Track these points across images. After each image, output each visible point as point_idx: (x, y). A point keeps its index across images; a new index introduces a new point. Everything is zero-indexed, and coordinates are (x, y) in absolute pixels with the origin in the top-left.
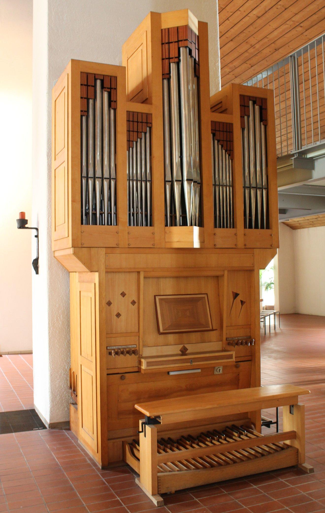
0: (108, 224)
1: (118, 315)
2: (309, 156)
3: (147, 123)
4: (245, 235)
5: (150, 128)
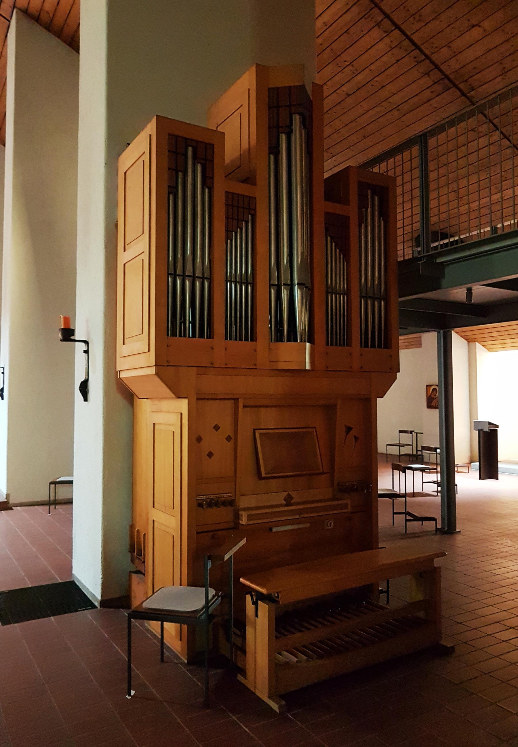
4: (361, 355)
5: (254, 217)
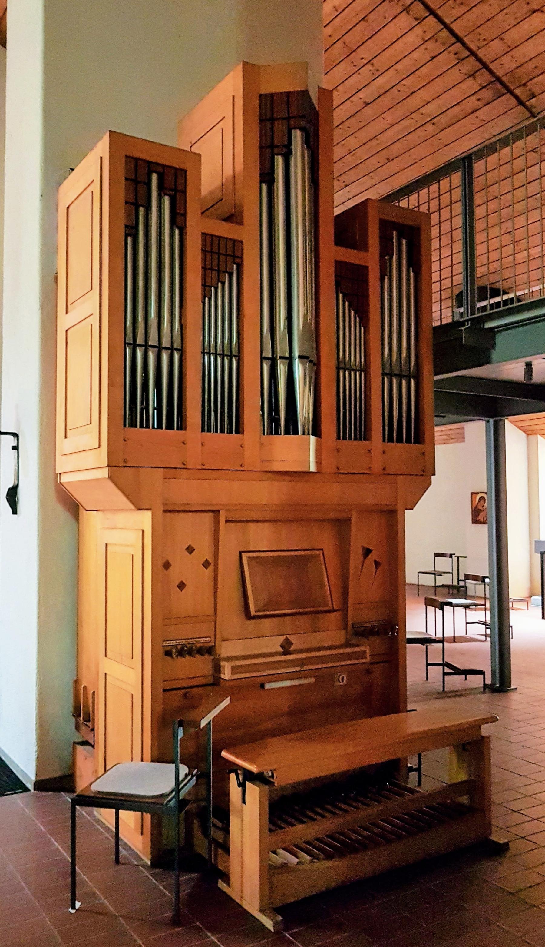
0: (142, 427)
1: (181, 586)
2: (489, 325)
3: (234, 257)
4: (384, 452)
